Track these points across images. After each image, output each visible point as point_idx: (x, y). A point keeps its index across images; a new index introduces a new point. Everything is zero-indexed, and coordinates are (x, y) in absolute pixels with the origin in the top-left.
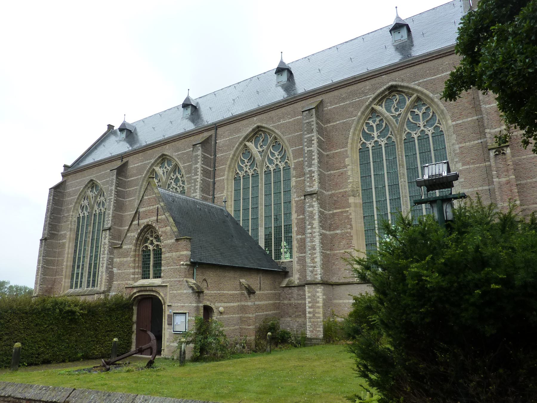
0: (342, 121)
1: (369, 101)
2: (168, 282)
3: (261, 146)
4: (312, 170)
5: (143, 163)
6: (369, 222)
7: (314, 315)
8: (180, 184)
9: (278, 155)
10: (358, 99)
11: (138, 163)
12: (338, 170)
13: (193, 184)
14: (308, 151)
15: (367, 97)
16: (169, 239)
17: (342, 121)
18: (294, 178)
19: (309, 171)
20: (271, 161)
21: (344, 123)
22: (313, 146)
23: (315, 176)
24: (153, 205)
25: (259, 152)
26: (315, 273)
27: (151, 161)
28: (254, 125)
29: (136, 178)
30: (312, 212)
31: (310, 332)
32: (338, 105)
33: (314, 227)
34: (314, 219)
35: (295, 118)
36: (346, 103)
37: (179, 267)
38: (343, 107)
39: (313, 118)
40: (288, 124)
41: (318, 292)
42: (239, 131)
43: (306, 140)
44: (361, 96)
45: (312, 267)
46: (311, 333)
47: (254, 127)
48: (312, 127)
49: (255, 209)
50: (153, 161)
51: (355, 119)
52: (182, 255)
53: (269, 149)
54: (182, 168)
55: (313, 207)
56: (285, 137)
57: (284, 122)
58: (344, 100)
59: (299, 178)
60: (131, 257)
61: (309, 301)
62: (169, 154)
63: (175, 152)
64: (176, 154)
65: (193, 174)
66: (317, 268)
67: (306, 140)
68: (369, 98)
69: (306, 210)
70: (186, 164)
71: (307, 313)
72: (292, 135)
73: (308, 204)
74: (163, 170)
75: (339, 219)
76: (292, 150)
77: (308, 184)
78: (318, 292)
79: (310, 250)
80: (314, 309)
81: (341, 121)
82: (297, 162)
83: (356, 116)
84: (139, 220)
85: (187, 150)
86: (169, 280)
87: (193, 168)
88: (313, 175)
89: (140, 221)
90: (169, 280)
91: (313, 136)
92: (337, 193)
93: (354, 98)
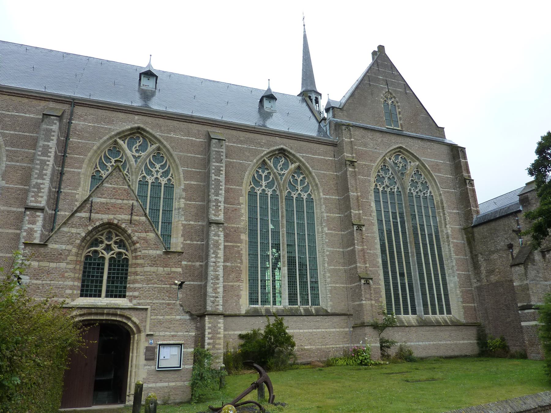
1: (264, 153)
2: (148, 304)
7: (214, 347)
16: (152, 249)
18: (184, 200)
22: (221, 176)
24: (124, 200)
25: (133, 156)
26: (216, 303)
30: (217, 241)
32: (236, 145)
34: (220, 249)
35: (188, 138)
37: (168, 286)
38: (240, 149)
39: (222, 149)
40: (179, 141)
45: (213, 297)
48: (222, 157)
57: (175, 136)
58: (241, 142)
66: (219, 299)
68: (264, 151)
70: (7, 132)
73: (214, 233)
77: (213, 212)
78: (219, 323)
79: (212, 279)
82: (188, 184)
83: (252, 161)
85: (13, 113)
86: (151, 301)
90: (151, 301)
91: (222, 167)
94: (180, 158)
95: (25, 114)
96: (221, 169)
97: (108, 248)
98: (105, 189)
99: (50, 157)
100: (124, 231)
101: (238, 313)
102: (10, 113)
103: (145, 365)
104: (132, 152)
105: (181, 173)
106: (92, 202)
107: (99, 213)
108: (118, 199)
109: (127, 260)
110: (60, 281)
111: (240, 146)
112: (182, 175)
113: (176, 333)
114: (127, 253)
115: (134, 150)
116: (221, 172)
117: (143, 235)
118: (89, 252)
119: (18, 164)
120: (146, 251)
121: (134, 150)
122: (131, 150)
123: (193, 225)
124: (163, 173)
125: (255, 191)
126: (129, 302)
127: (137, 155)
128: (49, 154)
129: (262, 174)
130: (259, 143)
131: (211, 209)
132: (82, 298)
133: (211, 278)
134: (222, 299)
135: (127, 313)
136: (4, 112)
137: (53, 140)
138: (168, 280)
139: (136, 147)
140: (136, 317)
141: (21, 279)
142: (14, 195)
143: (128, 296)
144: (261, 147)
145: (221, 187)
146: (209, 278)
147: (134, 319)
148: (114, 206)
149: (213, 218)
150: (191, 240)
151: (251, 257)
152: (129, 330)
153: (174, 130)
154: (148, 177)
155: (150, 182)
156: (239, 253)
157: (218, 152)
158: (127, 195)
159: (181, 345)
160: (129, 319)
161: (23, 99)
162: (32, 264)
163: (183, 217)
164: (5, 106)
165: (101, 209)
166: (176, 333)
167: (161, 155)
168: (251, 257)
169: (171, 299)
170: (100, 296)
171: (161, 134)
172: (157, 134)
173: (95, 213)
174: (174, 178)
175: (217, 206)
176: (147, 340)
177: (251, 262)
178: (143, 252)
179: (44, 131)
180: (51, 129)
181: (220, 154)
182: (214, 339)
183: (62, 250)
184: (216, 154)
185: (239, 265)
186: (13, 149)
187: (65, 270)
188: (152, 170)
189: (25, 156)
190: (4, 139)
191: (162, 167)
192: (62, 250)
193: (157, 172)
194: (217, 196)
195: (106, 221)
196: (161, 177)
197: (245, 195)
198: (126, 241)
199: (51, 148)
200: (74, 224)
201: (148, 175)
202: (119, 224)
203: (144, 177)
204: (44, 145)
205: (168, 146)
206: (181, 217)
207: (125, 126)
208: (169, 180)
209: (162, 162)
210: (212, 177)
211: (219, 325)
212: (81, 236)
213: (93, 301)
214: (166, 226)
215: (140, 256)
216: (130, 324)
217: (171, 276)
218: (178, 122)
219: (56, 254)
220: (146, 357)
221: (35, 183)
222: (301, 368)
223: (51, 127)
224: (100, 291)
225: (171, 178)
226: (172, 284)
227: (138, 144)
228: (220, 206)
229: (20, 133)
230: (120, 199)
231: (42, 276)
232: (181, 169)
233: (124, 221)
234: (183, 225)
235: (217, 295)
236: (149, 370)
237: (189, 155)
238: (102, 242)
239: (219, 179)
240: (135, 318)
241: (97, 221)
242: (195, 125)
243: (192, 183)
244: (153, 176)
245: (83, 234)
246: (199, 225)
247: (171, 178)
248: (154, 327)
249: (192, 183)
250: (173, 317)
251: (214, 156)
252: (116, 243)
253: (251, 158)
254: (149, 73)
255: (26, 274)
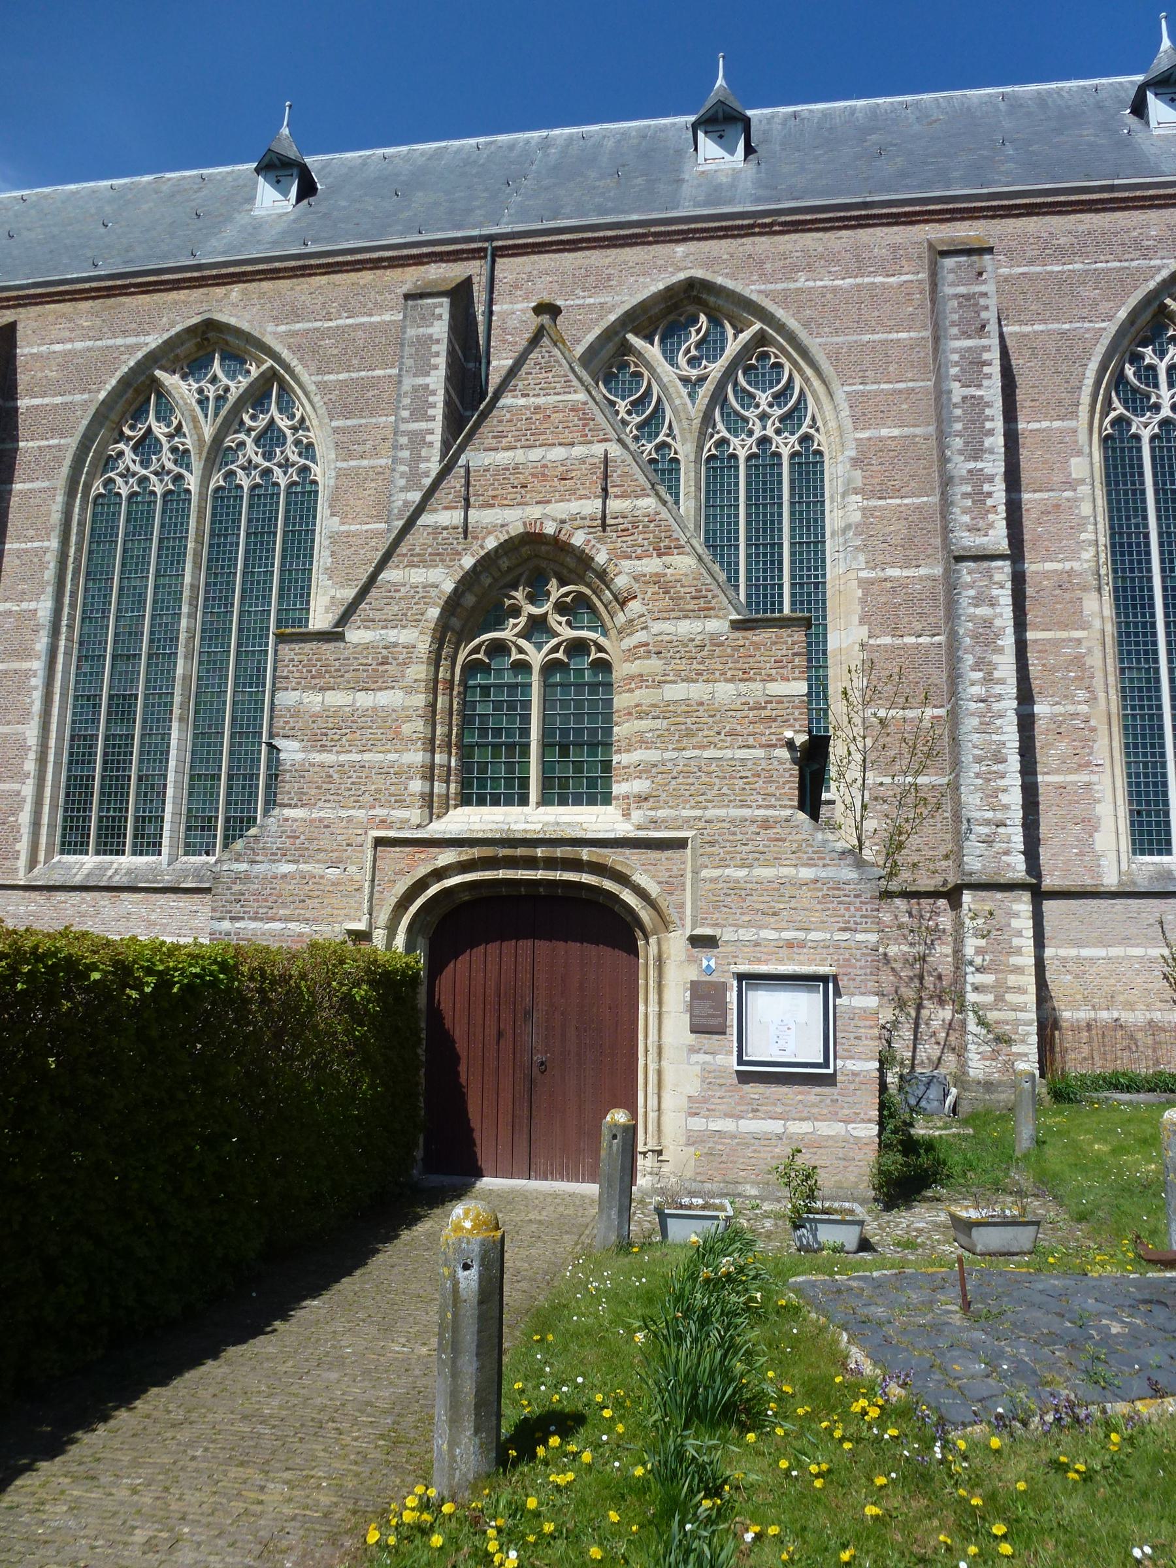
0: (1056, 326)
1: (1159, 278)
2: (687, 823)
3: (693, 362)
4: (981, 470)
5: (99, 343)
6: (1140, 689)
7: (999, 998)
8: (290, 455)
9: (771, 405)
10: (1117, 264)
11: (71, 340)
12: (1041, 491)
13: (405, 454)
14: (964, 398)
15: (1152, 263)
16: (686, 617)
17: (1056, 326)
18: (859, 498)
19: (970, 471)
20: (736, 422)
21: (1063, 333)
22: (986, 383)
23: (995, 495)
24: (572, 444)
25: (685, 380)
26: (998, 846)
27: (141, 339)
28: (673, 274)
29: (58, 400)
30: (987, 623)
31: (984, 1059)
32: (1038, 269)
33: (999, 679)
34: (1000, 651)
35: (859, 280)
36: (1070, 267)
37: (759, 753)
38: (1060, 281)
39: (984, 282)
40: (829, 296)
41: (1017, 915)
42: (603, 283)
43: (955, 357)
44: (1126, 256)
45: (988, 822)
46: (987, 1063)
47: (674, 279)
48: (984, 315)
49: (213, 634)
50: (153, 341)
51: (1105, 329)
52: (780, 699)
53: (733, 377)
54: (314, 388)
55: (993, 602)
56: (818, 340)
57: (811, 284)
58: (1061, 254)
59: (880, 498)
60: (409, 691)
61: (976, 947)
62: (245, 326)
63: (277, 320)
64: (282, 328)
65: (405, 414)
66: (1010, 830)
67: (955, 357)
68: (1159, 269)
69: (961, 612)
70: (332, 377)
71: (969, 988)
72: (850, 338)
73: (972, 593)
74: (200, 391)
75: (1044, 665)
76: (848, 393)
77: (966, 518)
78: (1017, 915)
79: (979, 760)
80: (1000, 976)
81: (1050, 326)
82: (869, 439)
83: (1109, 318)
84: (467, 506)
85: (340, 322)
86: (698, 813)
87: (409, 388)
88: (986, 488)
89: (471, 512)
90: (698, 813)
91: (987, 349)
92: (1037, 573)
93: (1102, 258)
94: (835, 356)
95: (371, 315)
96: (986, 356)
97: (537, 627)
98: (508, 416)
99: (433, 419)
100: (584, 560)
101: (1089, 882)
102: (331, 324)
103: (692, 1050)
104: (678, 368)
105: (844, 406)
106: (468, 471)
107: (493, 506)
108: (553, 445)
109: (603, 666)
110: (390, 751)
111: (1059, 268)
112: (846, 412)
113: (801, 935)
114: (602, 640)
115: (682, 360)
116: (986, 369)
117: (652, 565)
118: (476, 650)
119: (365, 463)
120: (666, 626)
121: (682, 360)
122: (672, 362)
123: (897, 579)
124: (782, 419)
125: (1133, 430)
126: (621, 818)
127: (694, 373)
128: (431, 412)
129: (1155, 361)
130: (1137, 244)
131: (956, 510)
132: (467, 809)
133: (974, 756)
134: (1020, 829)
135: (613, 857)
136: (318, 324)
137: (436, 367)
138: (760, 728)
139: (688, 351)
140: (645, 871)
141: (279, 750)
142: (362, 552)
143: (617, 798)
144: (1145, 257)
145: (988, 425)
146: (967, 758)
147: (640, 879)
148: (542, 473)
149: (968, 541)
150: (896, 632)
151: (1131, 680)
152: (629, 919)
153: (808, 264)
154: (734, 441)
155: (742, 454)
156: (1082, 666)
157: (968, 299)
158: (584, 425)
159: (824, 979)
160: (622, 879)
161: (360, 274)
162: (306, 700)
163: (862, 557)
164: (318, 307)
165: (500, 492)
166: (801, 935)
167: (773, 360)
168: (1131, 680)
169: (773, 801)
170: (524, 801)
171: (763, 287)
172: (752, 290)
173: (482, 506)
174: (822, 429)
175: (978, 497)
176: (691, 960)
177: (1133, 699)
178: (657, 627)
179: (412, 344)
180: (430, 337)
181: (976, 305)
182: (996, 971)
183: (386, 648)
184: (960, 305)
185: (1083, 708)
186: (349, 422)
187: (403, 714)
188: (746, 414)
189: (378, 437)
190: (326, 399)
191: (780, 398)
192: (386, 648)
193: (764, 417)
194: (976, 458)
195: (516, 529)
196: (778, 432)
197: (1086, 450)
198: (594, 598)
199: (434, 393)
200: (419, 555)
201: (735, 432)
202: (562, 537)
203: (723, 442)
204: (415, 389)
205: (792, 324)
206: (855, 558)
207: (646, 287)
208: (806, 439)
209: (778, 382)
210: (950, 392)
211: (1015, 923)
212: (441, 592)
213: (500, 818)
214: (809, 595)
215: (647, 645)
216: (628, 896)
217: (767, 713)
218: (820, 235)
219: (369, 661)
220: (697, 1021)
221: (401, 503)
222: (870, 825)
223: (430, 330)
224: (524, 783)
225: (812, 431)
226: (774, 746)
227: (694, 338)
228: (990, 494)
229: (363, 374)
230: (560, 444)
231: (336, 737)
232: (840, 393)
233: (579, 522)
234: (862, 582)
235: (1000, 816)
236: (708, 1068)
237: (866, 337)
238: (516, 611)
239: (981, 397)
240: (644, 877)
241: (489, 533)
242: (879, 232)
243: (884, 432)
244: (750, 433)
245: (448, 586)
246: (921, 578)
247: (812, 431)
248: (717, 908)
249: (884, 432)
250: (784, 871)
251: (955, 317)
252: (561, 608)
253: (1105, 307)
254: (721, 115)
255: (290, 733)
